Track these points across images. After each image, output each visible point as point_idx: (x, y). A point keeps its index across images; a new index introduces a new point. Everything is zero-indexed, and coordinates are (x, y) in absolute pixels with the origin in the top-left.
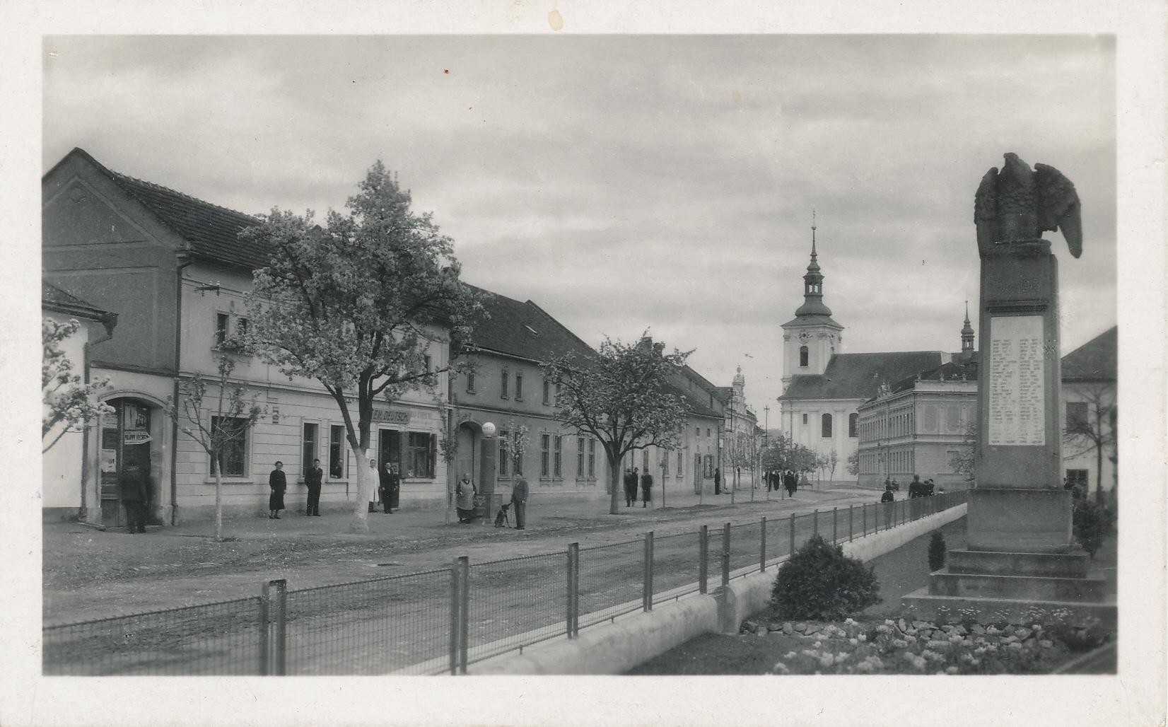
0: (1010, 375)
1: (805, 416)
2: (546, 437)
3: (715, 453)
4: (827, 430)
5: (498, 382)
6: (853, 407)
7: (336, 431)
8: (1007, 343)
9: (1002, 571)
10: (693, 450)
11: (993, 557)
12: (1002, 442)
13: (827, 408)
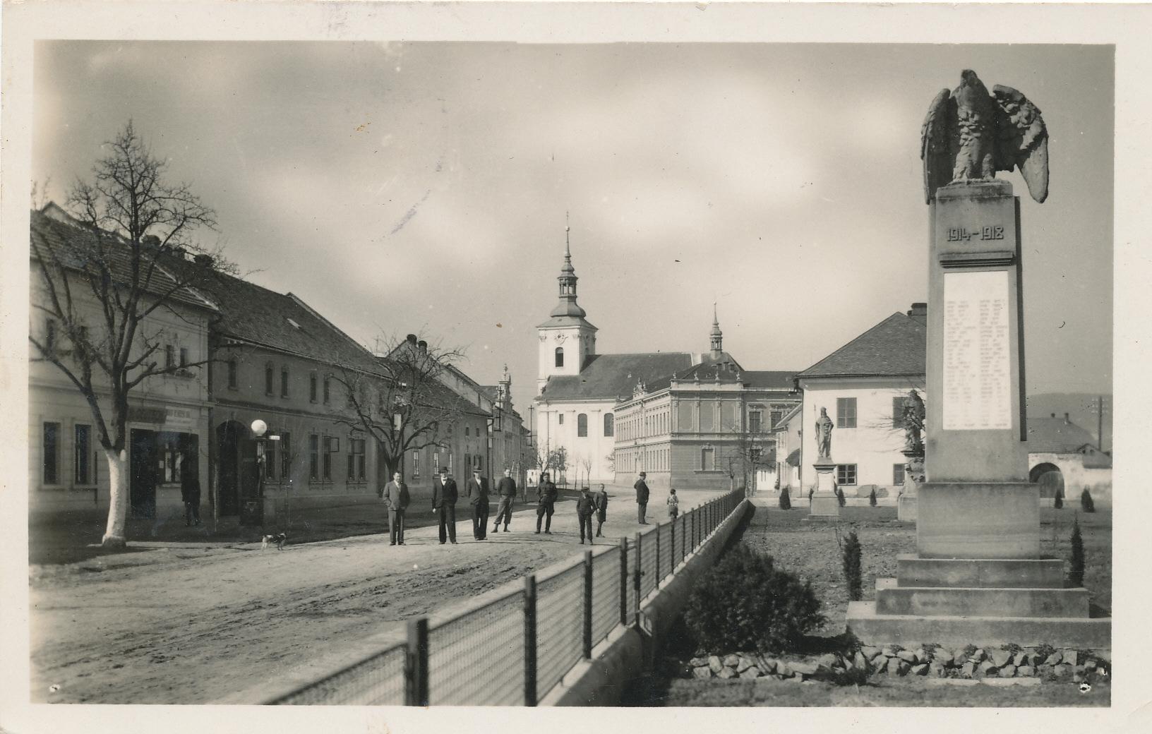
0: (967, 344)
1: (561, 416)
2: (314, 438)
3: (484, 454)
4: (582, 429)
5: (262, 377)
6: (608, 407)
7: (83, 430)
8: (963, 306)
9: (961, 583)
10: (463, 450)
11: (953, 565)
12: (959, 425)
13: (582, 408)
